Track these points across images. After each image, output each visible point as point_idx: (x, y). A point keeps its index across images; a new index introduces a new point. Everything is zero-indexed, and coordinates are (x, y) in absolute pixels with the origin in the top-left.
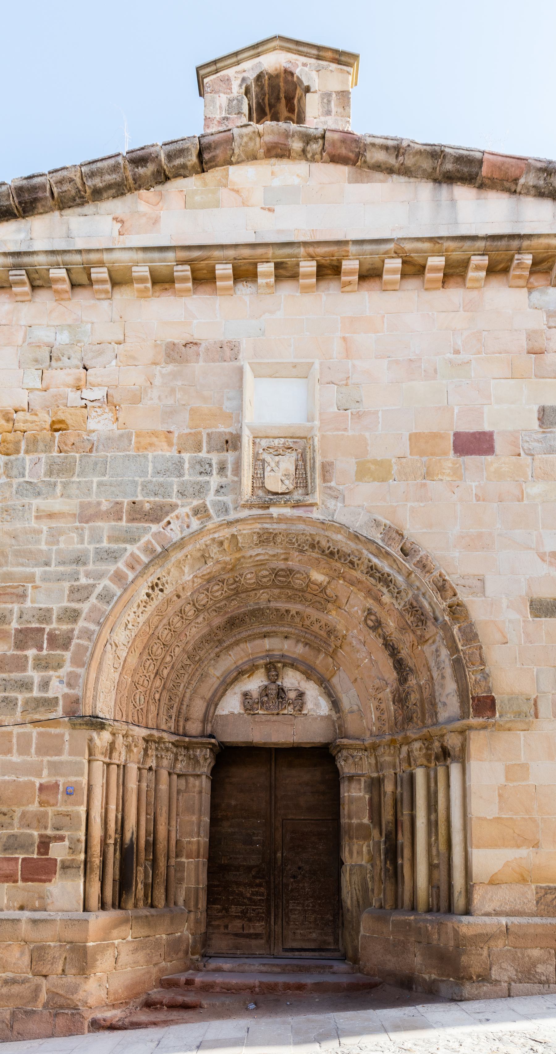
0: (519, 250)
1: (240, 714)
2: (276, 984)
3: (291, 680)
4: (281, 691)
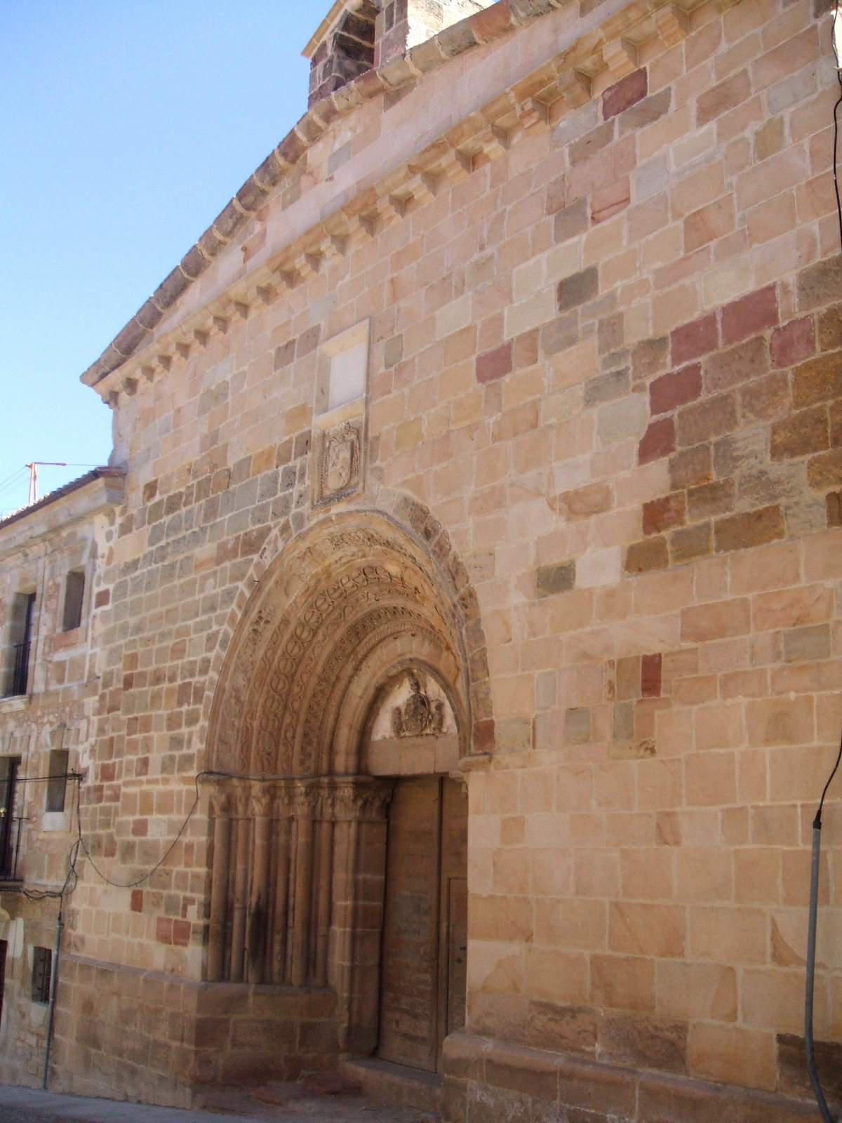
1: (391, 738)
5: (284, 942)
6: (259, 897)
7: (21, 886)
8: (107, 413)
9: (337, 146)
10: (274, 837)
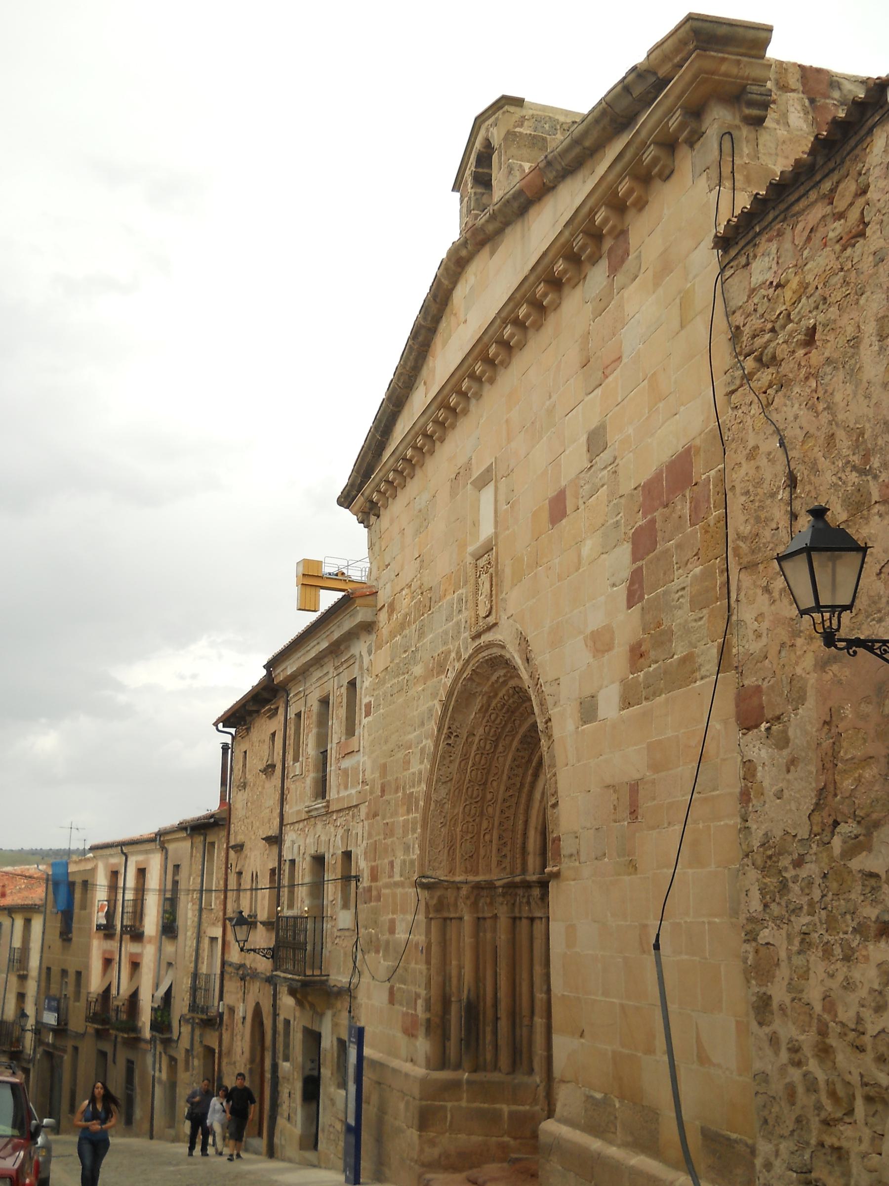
5: (495, 1033)
6: (469, 991)
7: (327, 980)
10: (481, 934)
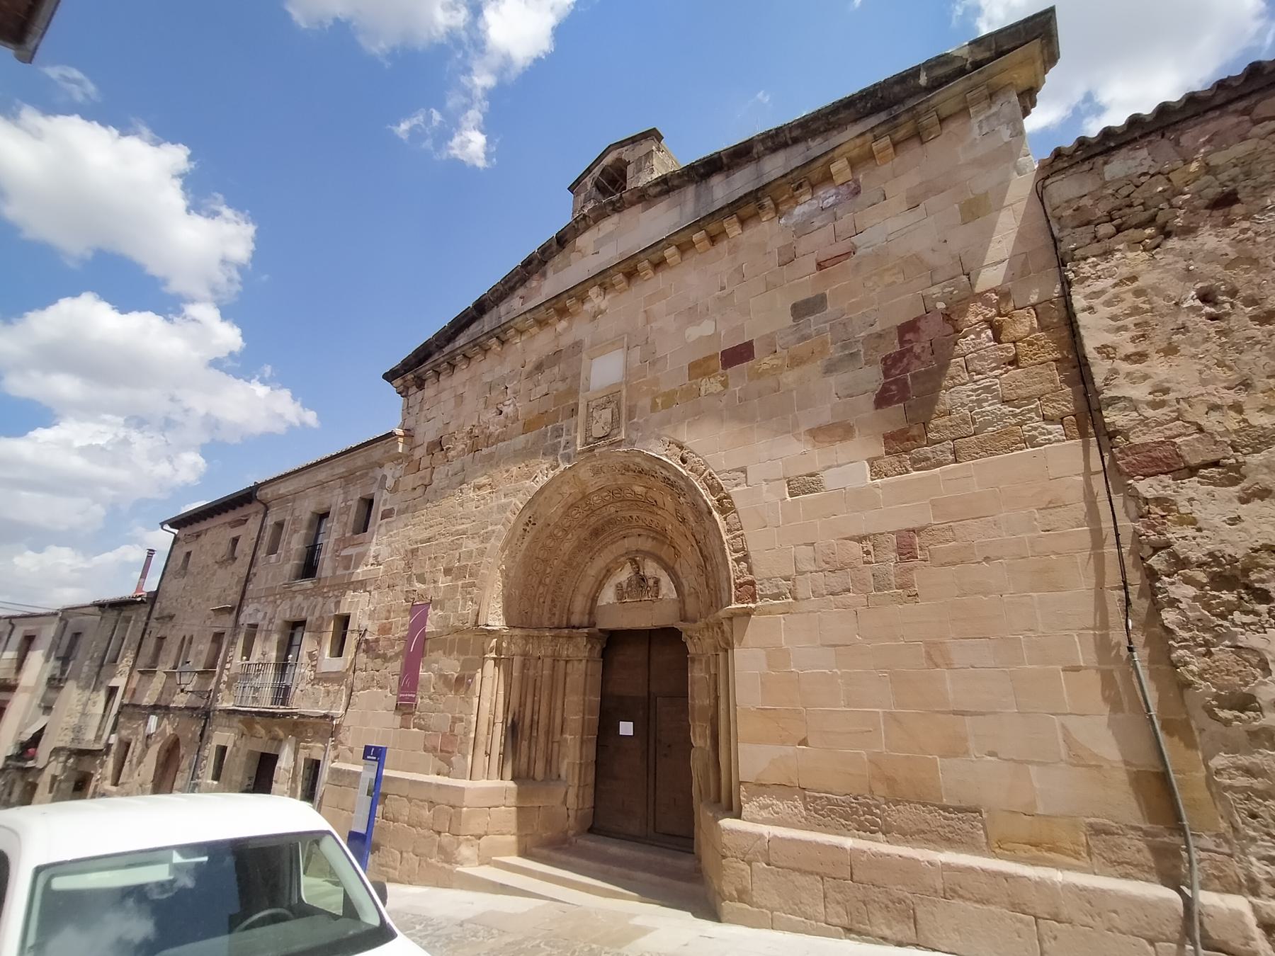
0: (832, 161)
2: (1181, 820)
3: (651, 569)
4: (643, 579)
8: (400, 400)
9: (601, 234)
